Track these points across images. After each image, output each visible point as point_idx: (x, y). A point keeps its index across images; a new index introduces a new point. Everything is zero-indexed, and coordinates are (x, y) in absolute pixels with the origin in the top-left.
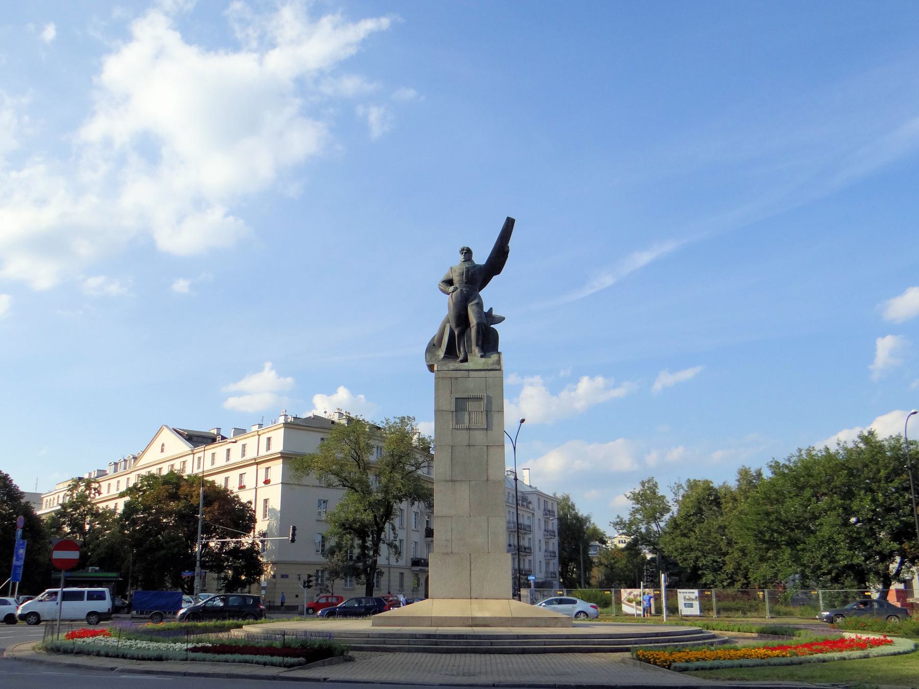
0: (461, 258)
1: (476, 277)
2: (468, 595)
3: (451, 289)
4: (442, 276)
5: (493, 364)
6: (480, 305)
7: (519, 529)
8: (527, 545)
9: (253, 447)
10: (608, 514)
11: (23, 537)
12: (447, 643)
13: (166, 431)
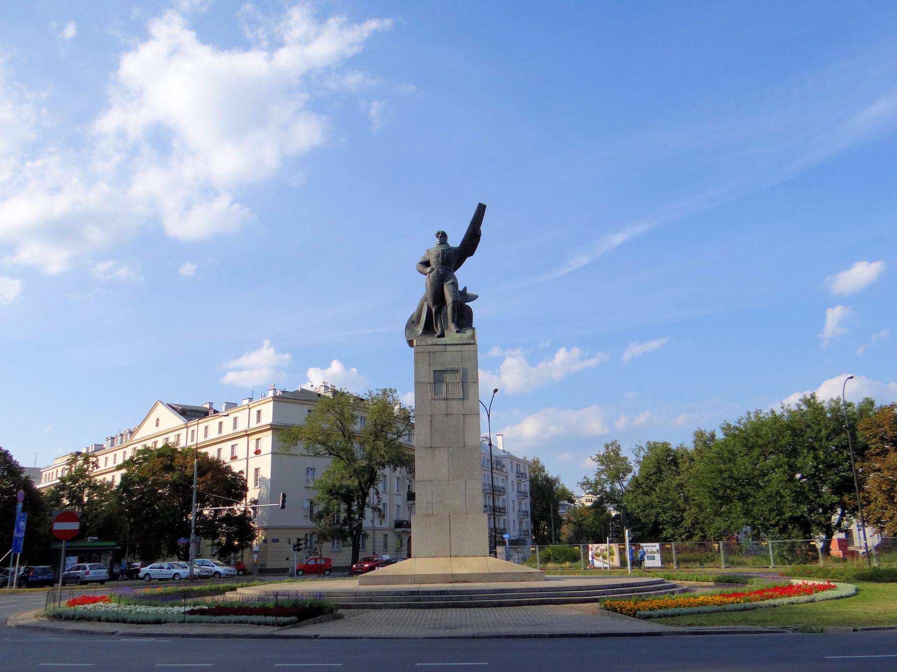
0: (437, 241)
1: (451, 259)
2: (449, 554)
3: (428, 270)
4: (420, 259)
5: (468, 339)
6: (455, 284)
7: (494, 491)
8: (501, 506)
9: (244, 419)
10: (575, 476)
12: (430, 599)
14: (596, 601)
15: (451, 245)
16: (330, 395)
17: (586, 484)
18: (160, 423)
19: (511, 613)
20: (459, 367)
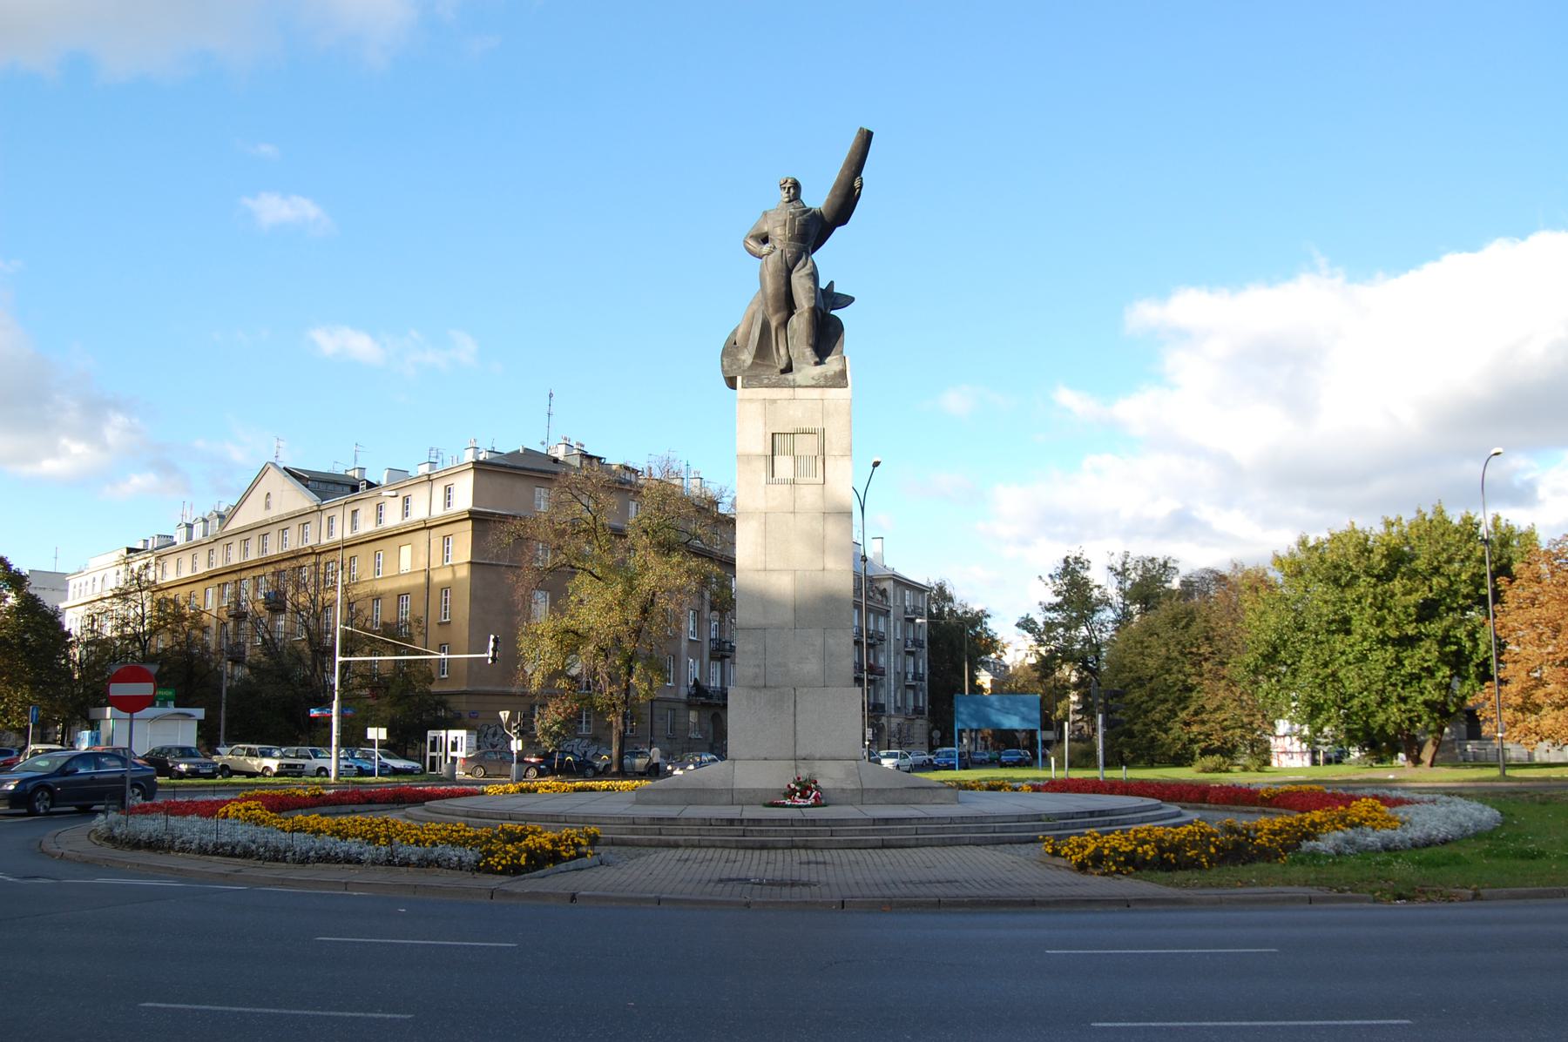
0: (784, 195)
1: (814, 231)
2: (799, 738)
3: (766, 248)
6: (814, 276)
7: (869, 643)
9: (424, 505)
10: (1009, 603)
11: (1231, 830)
13: (272, 472)
14: (1034, 840)
16: (576, 462)
18: (273, 500)
19: (877, 860)
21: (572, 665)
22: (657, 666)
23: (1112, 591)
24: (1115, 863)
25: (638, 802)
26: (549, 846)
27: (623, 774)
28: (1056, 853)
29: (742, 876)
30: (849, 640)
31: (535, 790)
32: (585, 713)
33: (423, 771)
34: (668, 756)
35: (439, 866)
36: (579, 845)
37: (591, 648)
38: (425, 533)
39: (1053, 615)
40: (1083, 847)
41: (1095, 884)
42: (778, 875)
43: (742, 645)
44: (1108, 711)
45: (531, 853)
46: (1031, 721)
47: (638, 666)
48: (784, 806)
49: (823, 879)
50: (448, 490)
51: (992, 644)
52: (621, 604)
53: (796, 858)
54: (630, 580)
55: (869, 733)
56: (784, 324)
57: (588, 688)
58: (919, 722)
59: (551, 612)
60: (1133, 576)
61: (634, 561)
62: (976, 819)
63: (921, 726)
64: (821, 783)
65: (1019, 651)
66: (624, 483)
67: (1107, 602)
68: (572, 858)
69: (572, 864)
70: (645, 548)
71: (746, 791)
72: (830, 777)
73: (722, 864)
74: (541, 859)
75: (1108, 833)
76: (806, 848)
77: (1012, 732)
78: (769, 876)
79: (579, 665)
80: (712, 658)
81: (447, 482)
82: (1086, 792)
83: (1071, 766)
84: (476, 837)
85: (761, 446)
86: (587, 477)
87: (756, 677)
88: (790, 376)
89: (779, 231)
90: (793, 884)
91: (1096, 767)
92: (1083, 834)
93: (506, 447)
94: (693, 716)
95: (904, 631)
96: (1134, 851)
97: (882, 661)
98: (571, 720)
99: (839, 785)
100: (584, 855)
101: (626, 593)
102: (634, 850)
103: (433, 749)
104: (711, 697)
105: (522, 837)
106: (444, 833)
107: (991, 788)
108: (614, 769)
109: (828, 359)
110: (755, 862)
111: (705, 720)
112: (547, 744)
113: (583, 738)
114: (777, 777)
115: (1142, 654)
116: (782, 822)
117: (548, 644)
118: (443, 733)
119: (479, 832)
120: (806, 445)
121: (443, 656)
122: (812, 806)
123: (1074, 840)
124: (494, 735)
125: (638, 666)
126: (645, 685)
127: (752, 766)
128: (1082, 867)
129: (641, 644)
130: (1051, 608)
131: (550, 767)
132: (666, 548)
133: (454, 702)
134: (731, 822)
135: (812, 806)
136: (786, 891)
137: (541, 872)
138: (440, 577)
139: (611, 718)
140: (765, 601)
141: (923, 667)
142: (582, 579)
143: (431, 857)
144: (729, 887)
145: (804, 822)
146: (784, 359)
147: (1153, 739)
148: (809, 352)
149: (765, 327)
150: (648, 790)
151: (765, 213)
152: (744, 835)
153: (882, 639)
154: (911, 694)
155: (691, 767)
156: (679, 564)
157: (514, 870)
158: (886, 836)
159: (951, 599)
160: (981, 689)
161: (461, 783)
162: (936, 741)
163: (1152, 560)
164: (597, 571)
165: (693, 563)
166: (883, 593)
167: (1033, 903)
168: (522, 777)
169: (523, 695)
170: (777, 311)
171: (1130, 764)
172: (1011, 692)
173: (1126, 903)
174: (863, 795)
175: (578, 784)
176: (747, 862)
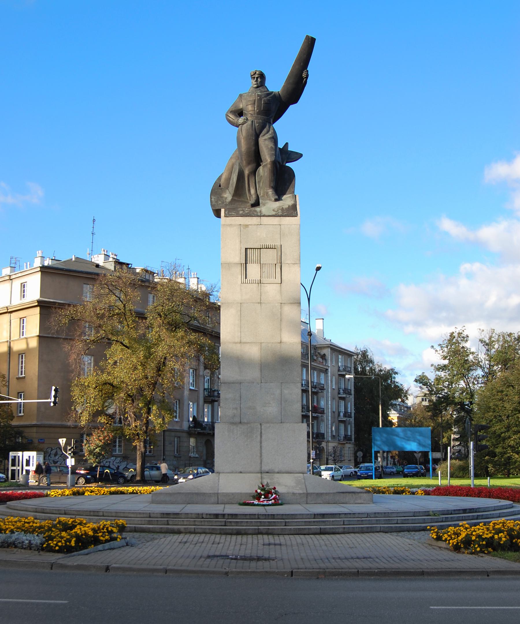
1: (274, 107)
2: (263, 457)
3: (241, 120)
4: (229, 106)
6: (274, 139)
10: (412, 360)
14: (424, 529)
15: (270, 90)
16: (111, 266)
17: (422, 380)
19: (316, 542)
20: (278, 244)
21: (109, 407)
22: (166, 407)
23: (482, 356)
24: (479, 546)
25: (153, 502)
26: (91, 533)
27: (144, 482)
28: (439, 538)
29: (224, 553)
30: (298, 391)
31: (83, 494)
32: (118, 441)
33: (6, 480)
34: (175, 469)
35: (16, 547)
36: (111, 532)
37: (122, 395)
38: (7, 315)
39: (442, 374)
40: (458, 534)
41: (466, 560)
42: (248, 553)
43: (225, 394)
44: (478, 440)
45: (78, 538)
46: (424, 446)
47: (154, 408)
48: (253, 505)
49: (279, 555)
50: (23, 285)
51: (399, 392)
52: (143, 365)
53: (261, 542)
54: (149, 348)
55: (313, 454)
56: (254, 172)
57: (120, 422)
58: (348, 445)
59: (95, 370)
60: (496, 346)
61: (151, 335)
62: (385, 514)
63: (349, 449)
64: (279, 489)
65: (415, 397)
66: (145, 282)
67: (478, 364)
68: (107, 541)
69: (107, 545)
70: (159, 326)
71: (227, 495)
72: (285, 484)
73: (210, 545)
74: (85, 542)
75: (475, 525)
76: (268, 534)
77: (412, 453)
78: (242, 553)
79: (114, 407)
80: (205, 402)
81: (23, 280)
82: (461, 495)
83: (452, 476)
84: (40, 527)
85: (237, 257)
86: (119, 278)
87: (234, 416)
88: (258, 209)
89: (250, 108)
90: (259, 559)
91: (469, 478)
92: (458, 525)
93: (64, 258)
94: (192, 441)
95: (338, 383)
96: (493, 537)
97: (322, 404)
98: (108, 445)
99: (291, 491)
100: (115, 539)
101: (146, 357)
102: (150, 535)
103: (13, 465)
104: (204, 428)
105: (73, 527)
106: (19, 524)
107: (396, 492)
108: (138, 478)
109: (284, 197)
110: (233, 543)
111: (199, 446)
112: (92, 461)
113: (116, 456)
114: (247, 484)
115: (501, 399)
116: (252, 516)
117: (92, 393)
118: (20, 454)
119: (43, 523)
120: (269, 256)
121: (19, 401)
122: (272, 505)
123: (451, 529)
124: (56, 455)
125: (154, 408)
126: (160, 421)
127: (231, 477)
128: (457, 548)
129: (151, 393)
130: (443, 368)
131: (94, 476)
132: (173, 326)
133: (27, 433)
134: (216, 516)
135: (272, 505)
136: (253, 564)
137: (86, 551)
138: (18, 346)
139: (136, 443)
140: (240, 362)
141: (351, 408)
142: (116, 348)
143: (10, 540)
144: (214, 562)
145: (267, 516)
146: (254, 197)
147: (509, 458)
148: (270, 192)
149: (241, 175)
150: (160, 494)
151: (241, 96)
152: (226, 525)
153: (322, 389)
154: (342, 426)
155: (191, 477)
156: (182, 338)
157: (67, 550)
158: (322, 526)
159: (371, 362)
160: (391, 424)
161: (33, 488)
162: (360, 459)
163: (510, 335)
164: (126, 342)
165: (193, 336)
166: (324, 357)
167: (422, 573)
168: (75, 483)
169: (76, 427)
170: (249, 164)
171: (492, 476)
172: (411, 425)
173: (487, 574)
174: (308, 497)
175: (113, 489)
176: (227, 543)
